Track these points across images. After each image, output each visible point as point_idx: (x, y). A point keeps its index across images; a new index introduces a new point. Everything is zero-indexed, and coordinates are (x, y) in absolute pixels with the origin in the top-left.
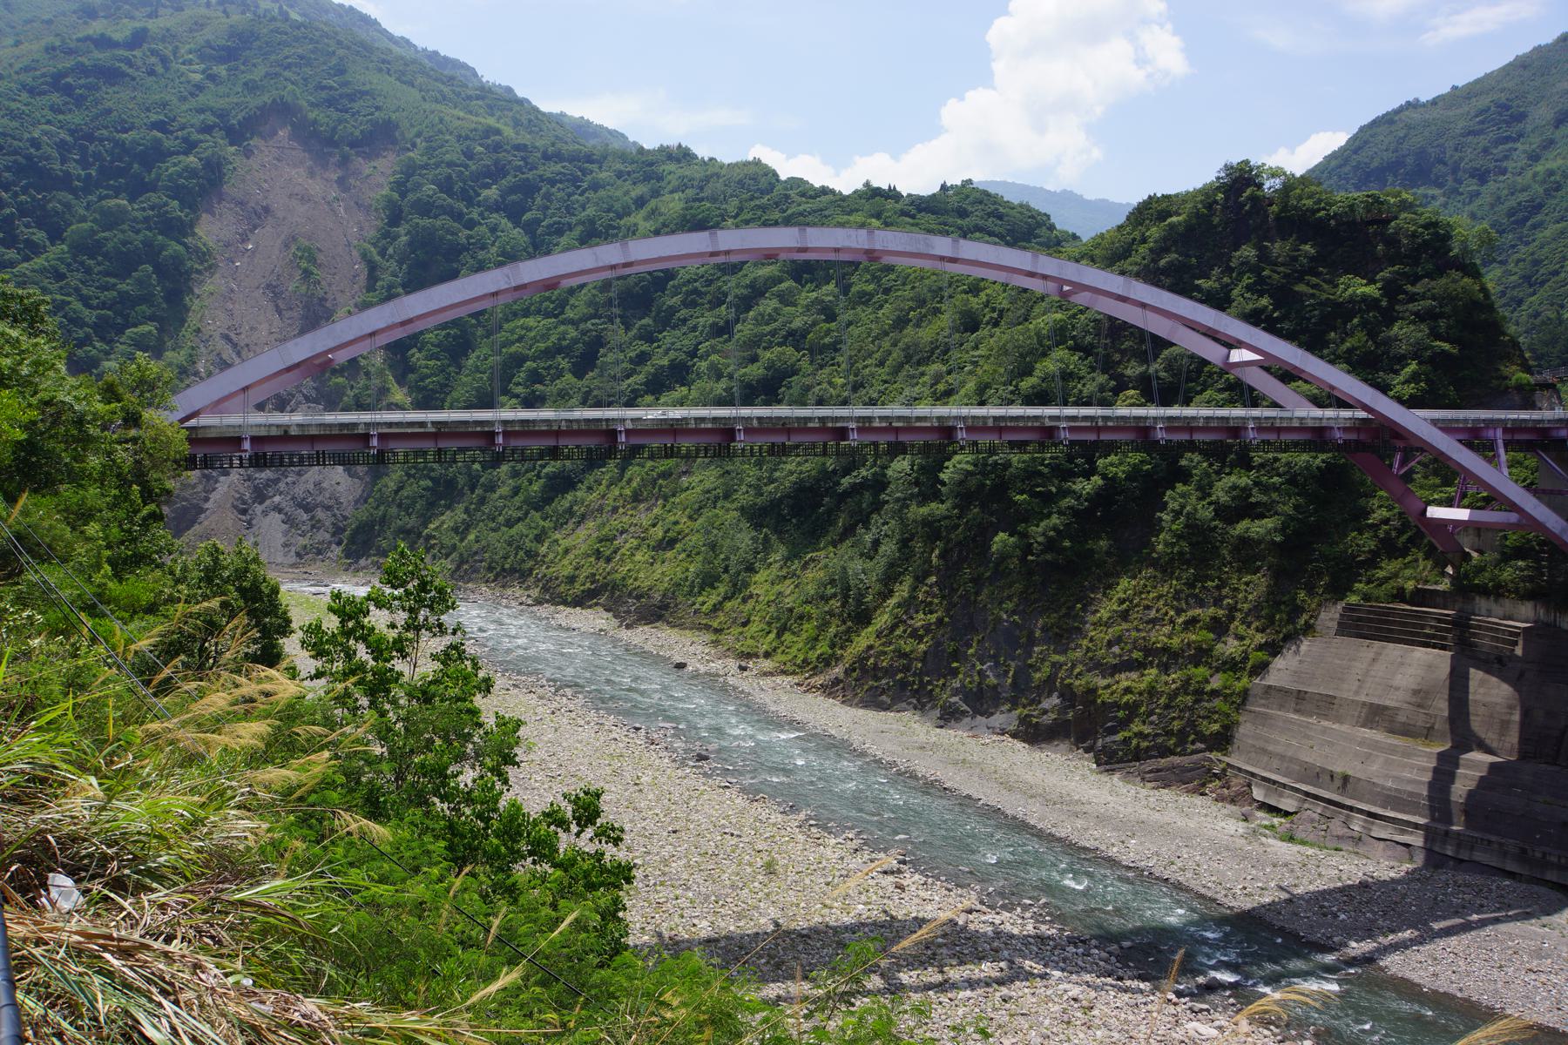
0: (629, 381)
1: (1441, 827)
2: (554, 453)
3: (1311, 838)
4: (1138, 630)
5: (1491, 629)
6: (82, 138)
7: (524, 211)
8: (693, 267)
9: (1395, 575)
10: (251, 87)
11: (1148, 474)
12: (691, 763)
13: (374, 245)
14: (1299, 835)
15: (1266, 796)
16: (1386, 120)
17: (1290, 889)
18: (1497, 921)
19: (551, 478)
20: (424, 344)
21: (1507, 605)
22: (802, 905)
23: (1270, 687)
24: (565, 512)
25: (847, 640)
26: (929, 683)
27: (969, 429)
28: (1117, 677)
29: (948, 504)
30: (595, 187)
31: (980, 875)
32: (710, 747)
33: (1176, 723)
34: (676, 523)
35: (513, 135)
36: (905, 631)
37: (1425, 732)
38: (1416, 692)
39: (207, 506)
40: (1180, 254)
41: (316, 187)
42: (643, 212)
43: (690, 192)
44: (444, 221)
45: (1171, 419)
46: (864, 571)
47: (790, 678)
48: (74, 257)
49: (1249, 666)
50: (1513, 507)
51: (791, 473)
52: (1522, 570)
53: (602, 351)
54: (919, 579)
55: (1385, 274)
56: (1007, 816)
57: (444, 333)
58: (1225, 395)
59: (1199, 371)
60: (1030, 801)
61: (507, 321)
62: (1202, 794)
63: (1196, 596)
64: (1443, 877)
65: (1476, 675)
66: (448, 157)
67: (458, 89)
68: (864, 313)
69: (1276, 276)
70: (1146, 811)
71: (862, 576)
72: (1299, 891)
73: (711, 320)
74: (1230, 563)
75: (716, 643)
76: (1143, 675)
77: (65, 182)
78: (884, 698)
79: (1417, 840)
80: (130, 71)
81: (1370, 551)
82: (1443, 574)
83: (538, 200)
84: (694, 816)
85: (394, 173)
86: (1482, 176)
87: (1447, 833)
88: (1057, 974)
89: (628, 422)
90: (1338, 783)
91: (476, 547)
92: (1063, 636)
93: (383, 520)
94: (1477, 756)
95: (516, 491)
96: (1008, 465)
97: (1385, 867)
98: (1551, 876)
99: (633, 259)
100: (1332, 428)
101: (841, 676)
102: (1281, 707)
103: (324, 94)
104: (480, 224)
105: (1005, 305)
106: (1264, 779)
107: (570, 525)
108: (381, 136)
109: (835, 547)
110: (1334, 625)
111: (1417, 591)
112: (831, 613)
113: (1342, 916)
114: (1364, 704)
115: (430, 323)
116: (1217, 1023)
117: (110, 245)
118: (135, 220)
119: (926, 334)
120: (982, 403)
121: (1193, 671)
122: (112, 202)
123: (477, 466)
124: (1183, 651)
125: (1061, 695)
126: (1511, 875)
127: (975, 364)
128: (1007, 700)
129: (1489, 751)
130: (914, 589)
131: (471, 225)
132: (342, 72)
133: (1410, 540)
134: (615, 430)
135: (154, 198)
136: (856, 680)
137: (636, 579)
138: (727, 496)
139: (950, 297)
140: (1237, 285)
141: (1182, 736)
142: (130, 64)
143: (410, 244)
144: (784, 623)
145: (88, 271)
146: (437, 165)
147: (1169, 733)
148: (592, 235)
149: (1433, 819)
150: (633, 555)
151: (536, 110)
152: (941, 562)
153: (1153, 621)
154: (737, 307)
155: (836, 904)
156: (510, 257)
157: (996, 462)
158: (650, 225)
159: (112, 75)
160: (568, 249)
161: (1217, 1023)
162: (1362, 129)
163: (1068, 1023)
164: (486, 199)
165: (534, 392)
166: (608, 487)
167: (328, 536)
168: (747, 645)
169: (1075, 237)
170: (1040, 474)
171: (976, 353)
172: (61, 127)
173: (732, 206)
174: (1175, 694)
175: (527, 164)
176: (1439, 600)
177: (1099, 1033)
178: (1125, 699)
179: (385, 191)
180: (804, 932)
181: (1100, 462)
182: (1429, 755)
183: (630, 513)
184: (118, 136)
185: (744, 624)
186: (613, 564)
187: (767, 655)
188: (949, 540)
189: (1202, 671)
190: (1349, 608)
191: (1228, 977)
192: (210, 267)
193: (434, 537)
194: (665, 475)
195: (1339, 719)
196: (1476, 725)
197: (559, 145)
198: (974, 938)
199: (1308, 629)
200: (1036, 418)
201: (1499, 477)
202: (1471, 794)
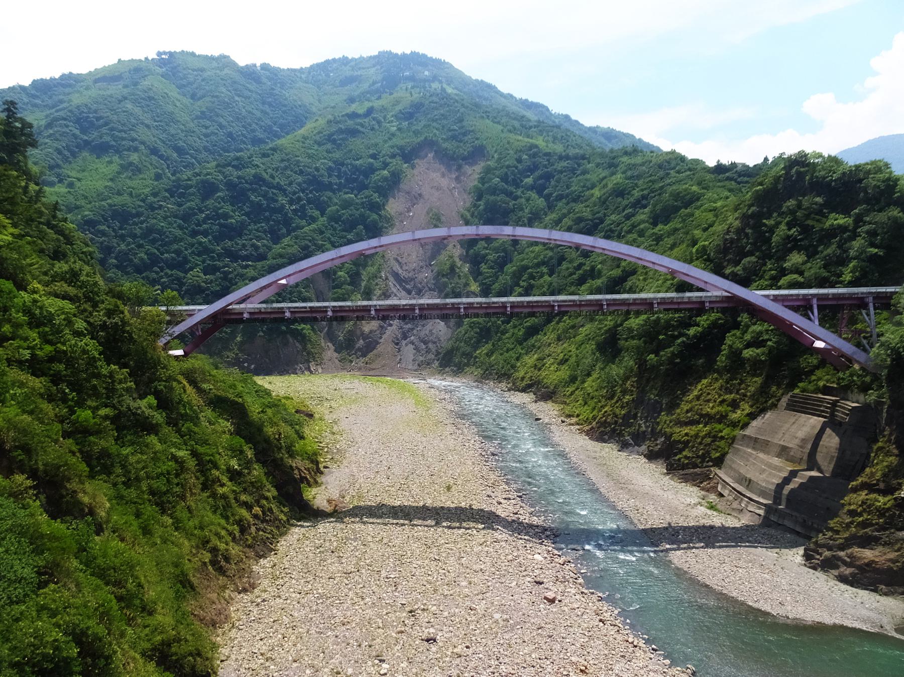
2: (532, 314)
6: (339, 164)
10: (417, 133)
13: (469, 211)
19: (528, 328)
20: (487, 261)
26: (624, 430)
34: (570, 351)
39: (381, 341)
41: (444, 182)
44: (502, 197)
48: (329, 223)
65: (828, 431)
66: (507, 163)
77: (329, 187)
80: (361, 129)
83: (553, 183)
85: (480, 173)
92: (673, 406)
102: (747, 446)
103: (450, 134)
108: (478, 153)
114: (780, 445)
117: (345, 217)
118: (357, 204)
122: (347, 196)
131: (516, 198)
135: (366, 192)
141: (703, 457)
142: (362, 126)
143: (484, 210)
145: (335, 229)
146: (502, 168)
147: (698, 457)
159: (353, 133)
164: (526, 184)
167: (433, 356)
172: (330, 160)
175: (549, 162)
179: (476, 183)
184: (353, 162)
189: (719, 427)
192: (392, 225)
195: (768, 453)
196: (819, 457)
199: (774, 406)
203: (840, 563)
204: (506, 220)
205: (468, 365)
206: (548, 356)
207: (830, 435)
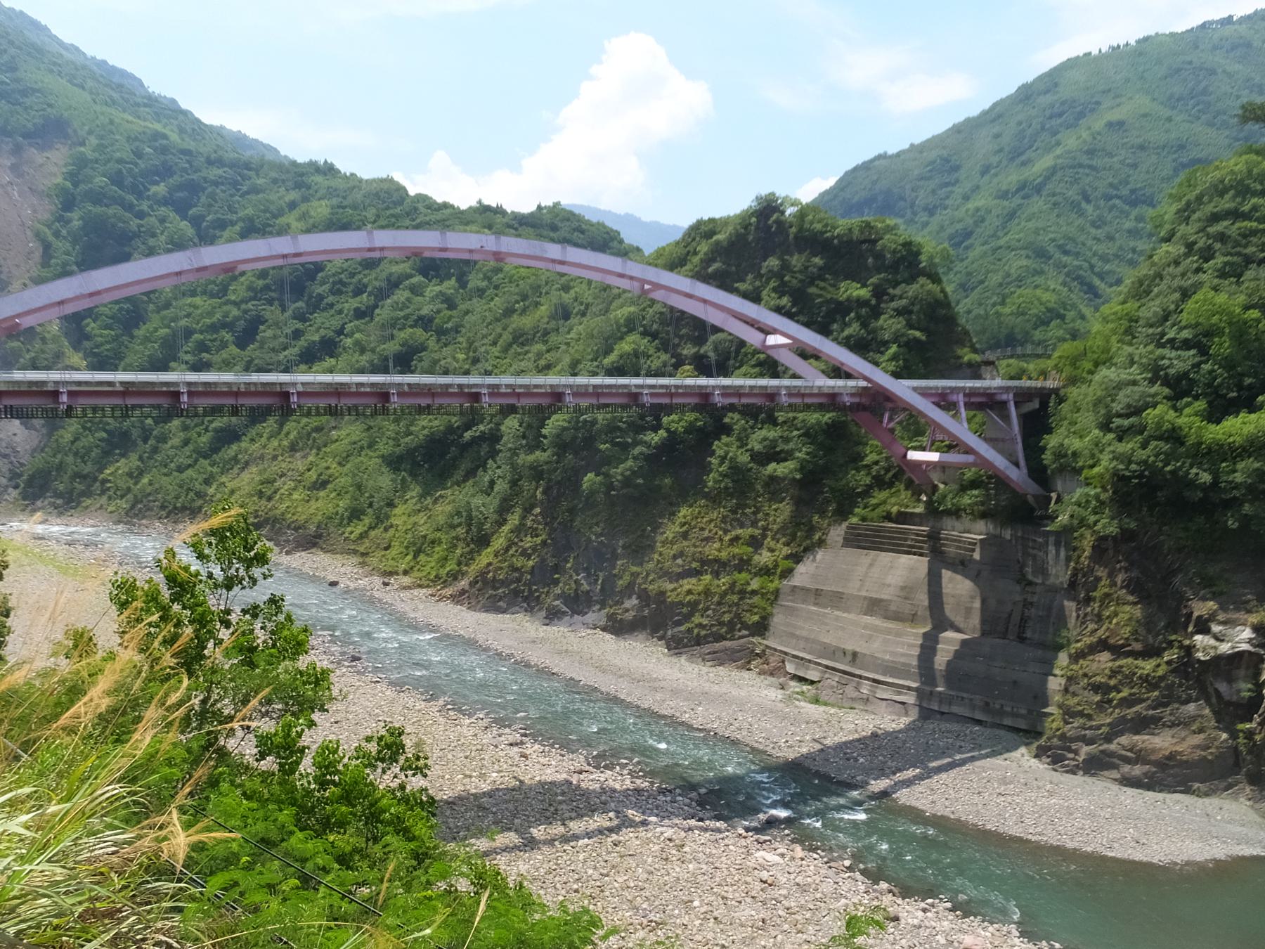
0: (286, 353)
1: (928, 689)
3: (832, 700)
4: (695, 546)
5: (955, 541)
7: (191, 206)
8: (338, 261)
9: (884, 502)
11: (700, 430)
12: (346, 664)
13: (49, 227)
14: (823, 698)
15: (796, 669)
16: (865, 167)
17: (822, 740)
18: (973, 759)
21: (966, 521)
22: (447, 776)
23: (795, 587)
24: (230, 459)
25: (471, 559)
27: (575, 395)
28: (680, 581)
29: (549, 452)
30: (255, 190)
31: (587, 742)
32: (362, 650)
33: (726, 615)
34: (328, 468)
35: (180, 141)
36: (517, 551)
37: (911, 617)
38: (903, 588)
40: (724, 264)
42: (296, 213)
43: (335, 201)
45: (724, 387)
46: (485, 505)
47: (425, 590)
49: (779, 570)
50: (969, 450)
51: (424, 428)
52: (977, 497)
53: (262, 327)
54: (528, 510)
55: (873, 280)
56: (602, 693)
57: (117, 307)
58: (757, 370)
59: (737, 352)
60: (620, 680)
61: (176, 299)
62: (749, 670)
63: (738, 520)
64: (931, 726)
65: (946, 574)
66: (118, 155)
67: (126, 96)
68: (477, 304)
69: (795, 282)
70: (707, 684)
71: (482, 509)
72: (828, 742)
73: (356, 305)
74: (762, 495)
75: (363, 564)
76: (700, 580)
78: (501, 603)
79: (910, 699)
81: (867, 485)
82: (919, 501)
83: (203, 199)
84: (352, 708)
85: (66, 165)
86: (931, 211)
87: (931, 693)
88: (653, 819)
89: (300, 386)
90: (849, 658)
91: (149, 489)
92: (640, 550)
93: (60, 467)
94: (950, 634)
95: (186, 442)
96: (594, 422)
97: (891, 721)
98: (1008, 721)
99: (302, 251)
100: (841, 394)
101: (467, 587)
102: (804, 602)
104: (150, 215)
105: (590, 300)
106: (794, 656)
107: (236, 470)
109: (459, 486)
110: (841, 540)
111: (900, 513)
112: (457, 538)
113: (861, 760)
114: (865, 598)
115: (107, 298)
116: (779, 851)
119: (524, 322)
120: (575, 375)
121: (737, 575)
123: (149, 421)
124: (730, 561)
125: (639, 597)
126: (979, 722)
127: (568, 344)
128: (597, 602)
129: (958, 630)
130: (523, 518)
131: (141, 215)
132: (13, 69)
133: (895, 476)
134: (288, 392)
136: (479, 590)
137: (293, 514)
138: (370, 446)
139: (547, 293)
140: (765, 288)
141: (731, 626)
144: (418, 548)
148: (251, 230)
149: (922, 683)
150: (291, 494)
151: (198, 121)
152: (545, 497)
153: (707, 539)
154: (376, 297)
155: (474, 774)
156: (178, 245)
157: (585, 421)
158: (301, 225)
160: (230, 240)
161: (779, 851)
162: (846, 173)
163: (666, 859)
164: (155, 194)
165: (201, 359)
166: (268, 439)
168: (390, 565)
169: (638, 249)
170: (619, 429)
171: (569, 337)
173: (370, 214)
174: (725, 593)
175: (191, 166)
176: (917, 520)
177: (690, 866)
178: (688, 598)
179: (59, 180)
180: (450, 800)
181: (665, 420)
182: (915, 635)
183: (288, 460)
185: (386, 549)
186: (273, 502)
187: (406, 573)
188: (550, 480)
189: (744, 575)
190: (851, 527)
191: (783, 813)
193: (109, 481)
194: (318, 429)
196: (949, 611)
197: (220, 153)
198: (586, 794)
199: (821, 543)
200: (625, 386)
201: (960, 428)
202: (949, 663)
203: (1116, 761)
204: (127, 249)
205: (87, 493)
206: (281, 477)
207: (951, 580)
